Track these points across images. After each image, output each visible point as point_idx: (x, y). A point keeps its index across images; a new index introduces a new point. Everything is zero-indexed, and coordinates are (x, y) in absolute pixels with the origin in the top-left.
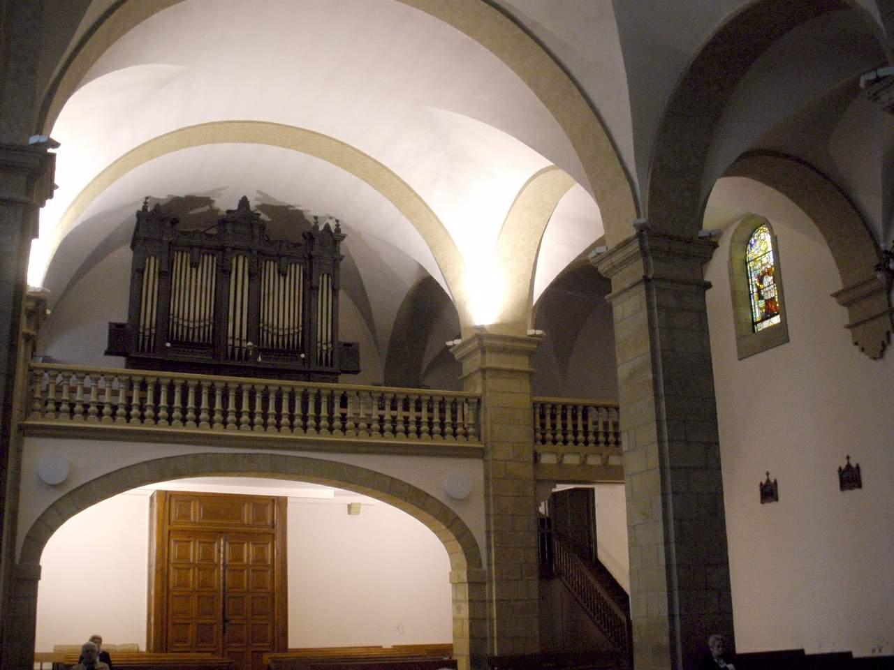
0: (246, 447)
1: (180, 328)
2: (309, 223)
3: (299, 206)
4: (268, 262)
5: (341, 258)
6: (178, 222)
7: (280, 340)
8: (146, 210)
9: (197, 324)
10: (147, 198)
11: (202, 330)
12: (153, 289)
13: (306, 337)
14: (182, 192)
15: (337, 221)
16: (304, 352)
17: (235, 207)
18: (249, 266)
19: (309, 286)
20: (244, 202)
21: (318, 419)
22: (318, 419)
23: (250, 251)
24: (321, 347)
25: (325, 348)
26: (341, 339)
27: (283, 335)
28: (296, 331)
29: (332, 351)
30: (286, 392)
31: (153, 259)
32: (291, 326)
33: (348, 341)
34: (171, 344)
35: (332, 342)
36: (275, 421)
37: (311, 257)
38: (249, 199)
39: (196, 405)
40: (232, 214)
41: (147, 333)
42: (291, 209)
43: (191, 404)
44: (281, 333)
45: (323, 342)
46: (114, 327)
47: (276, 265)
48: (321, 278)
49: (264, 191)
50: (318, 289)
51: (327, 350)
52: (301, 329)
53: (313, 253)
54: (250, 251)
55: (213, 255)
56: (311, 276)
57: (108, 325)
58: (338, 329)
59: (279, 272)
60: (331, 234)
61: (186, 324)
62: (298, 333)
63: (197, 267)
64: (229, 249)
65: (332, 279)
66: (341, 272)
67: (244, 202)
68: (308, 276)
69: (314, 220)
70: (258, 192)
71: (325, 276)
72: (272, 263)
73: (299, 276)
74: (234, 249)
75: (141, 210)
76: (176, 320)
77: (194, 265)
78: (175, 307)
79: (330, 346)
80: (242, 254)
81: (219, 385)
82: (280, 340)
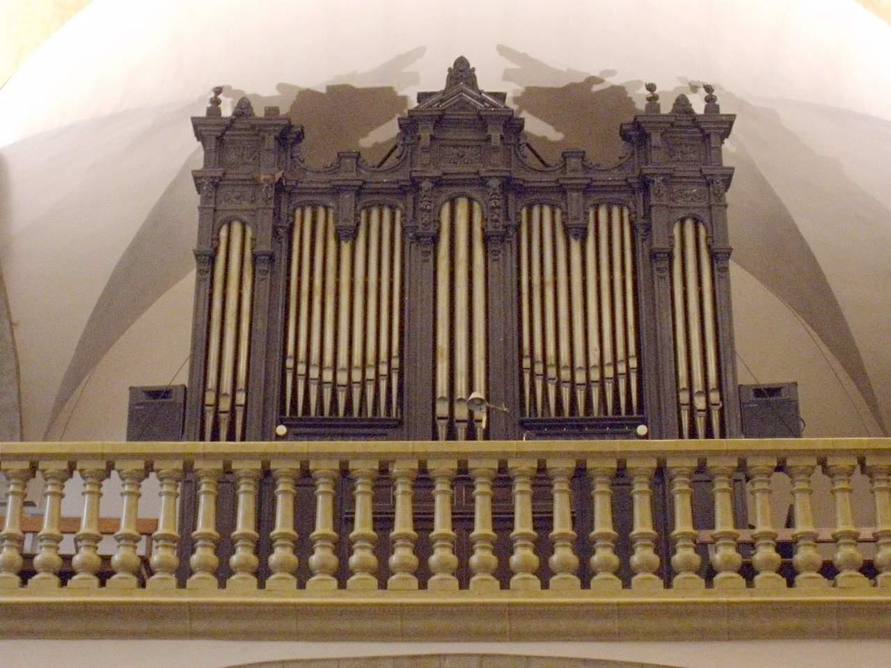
0: (404, 636)
1: (314, 389)
2: (630, 102)
3: (612, 73)
4: (536, 211)
5: (727, 178)
6: (300, 137)
7: (580, 396)
8: (219, 111)
9: (357, 376)
10: (218, 91)
11: (356, 392)
12: (240, 296)
13: (649, 386)
14: (317, 79)
15: (709, 89)
16: (644, 422)
17: (437, 83)
18: (484, 219)
19: (646, 252)
20: (461, 73)
21: (624, 546)
22: (624, 546)
23: (483, 182)
24: (691, 404)
25: (700, 403)
26: (744, 379)
27: (588, 384)
28: (622, 369)
29: (722, 411)
30: (523, 474)
31: (237, 227)
32: (608, 358)
33: (766, 380)
34: (287, 426)
35: (720, 388)
36: (493, 560)
37: (645, 184)
38: (507, 95)
39: (258, 528)
40: (429, 101)
41: (225, 405)
42: (596, 88)
43: (244, 524)
44: (580, 377)
45: (696, 390)
46: (143, 398)
47: (558, 212)
48: (676, 231)
49: (520, 49)
50: (670, 257)
51: (708, 411)
52: (633, 363)
53: (648, 170)
54: (483, 182)
55: (393, 208)
56: (648, 229)
57: (127, 393)
58: (733, 353)
59: (566, 230)
60: (695, 120)
61: (328, 376)
62: (628, 375)
63: (354, 237)
64: (426, 185)
65: (707, 231)
66: (730, 212)
67: (461, 73)
68: (641, 230)
69: (648, 93)
70: (503, 50)
71: (689, 224)
72: (547, 210)
73: (621, 234)
74: (438, 183)
75: (203, 114)
76: (301, 369)
77: (347, 234)
78: (299, 336)
79: (714, 397)
80: (462, 195)
81: (324, 469)
82: (580, 396)
